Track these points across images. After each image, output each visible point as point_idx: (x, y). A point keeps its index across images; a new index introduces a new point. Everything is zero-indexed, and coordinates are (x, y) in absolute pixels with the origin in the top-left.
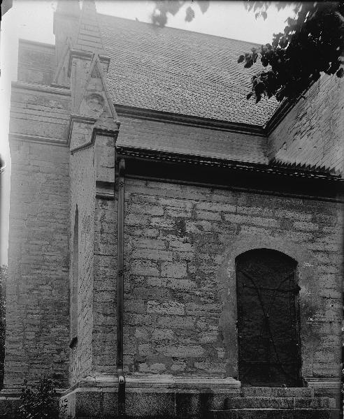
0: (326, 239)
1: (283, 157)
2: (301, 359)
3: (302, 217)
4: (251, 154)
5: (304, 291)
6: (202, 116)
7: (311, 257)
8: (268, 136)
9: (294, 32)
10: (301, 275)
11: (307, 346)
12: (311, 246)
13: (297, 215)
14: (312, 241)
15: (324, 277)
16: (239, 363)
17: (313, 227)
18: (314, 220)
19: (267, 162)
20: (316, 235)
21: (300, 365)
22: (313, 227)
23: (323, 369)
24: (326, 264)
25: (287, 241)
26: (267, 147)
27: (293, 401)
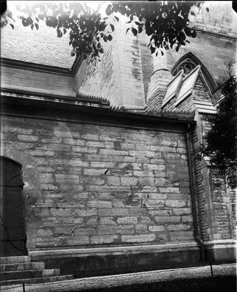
0: (45, 148)
1: (84, 91)
2: (26, 235)
3: (24, 131)
4: (61, 90)
5: (26, 185)
6: (23, 60)
7: (32, 161)
8: (74, 77)
9: (144, 9)
10: (24, 175)
11: (30, 226)
12: (33, 153)
13: (20, 130)
14: (33, 149)
15: (44, 176)
16: (228, 248)
17: (34, 139)
18: (33, 134)
19: (74, 95)
20: (36, 145)
21: (25, 240)
22: (34, 139)
23: (44, 242)
24: (45, 166)
25: (12, 150)
26: (74, 85)
27: (3, 267)
